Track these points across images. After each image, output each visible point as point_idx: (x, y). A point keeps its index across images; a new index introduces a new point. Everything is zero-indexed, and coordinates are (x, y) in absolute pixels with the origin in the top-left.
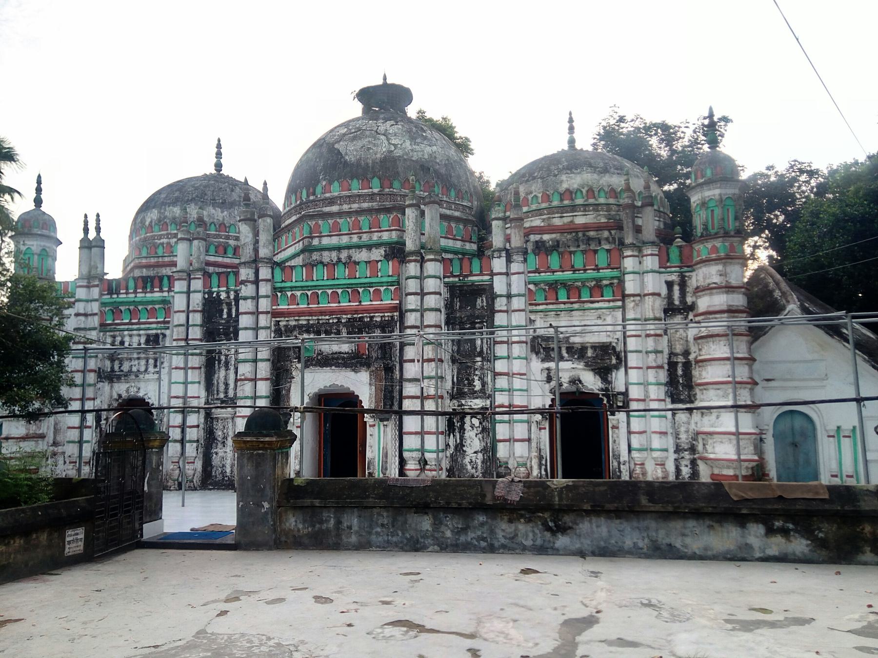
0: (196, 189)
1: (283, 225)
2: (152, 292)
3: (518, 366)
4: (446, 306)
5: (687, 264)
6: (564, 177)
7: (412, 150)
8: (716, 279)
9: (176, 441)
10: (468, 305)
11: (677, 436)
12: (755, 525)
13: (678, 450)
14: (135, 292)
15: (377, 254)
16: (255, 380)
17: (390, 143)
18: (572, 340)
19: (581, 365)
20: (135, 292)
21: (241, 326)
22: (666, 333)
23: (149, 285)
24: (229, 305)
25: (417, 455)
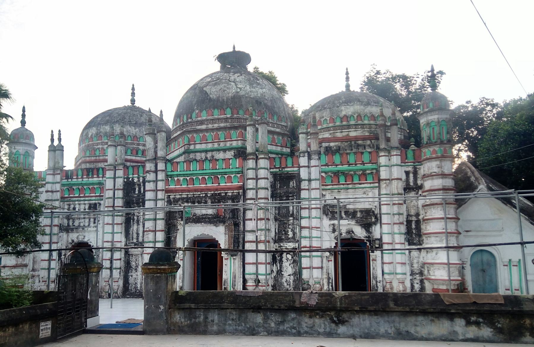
0: (119, 115)
1: (172, 137)
2: (92, 177)
3: (315, 223)
4: (271, 186)
5: (418, 161)
6: (343, 108)
7: (251, 91)
8: (436, 170)
9: (107, 268)
10: (285, 186)
11: (412, 265)
12: (459, 319)
13: (412, 274)
14: (82, 178)
15: (229, 155)
16: (155, 231)
17: (237, 87)
18: (348, 207)
19: (353, 222)
20: (82, 178)
21: (146, 198)
22: (405, 203)
23: (90, 173)
24: (139, 185)
25: (254, 277)
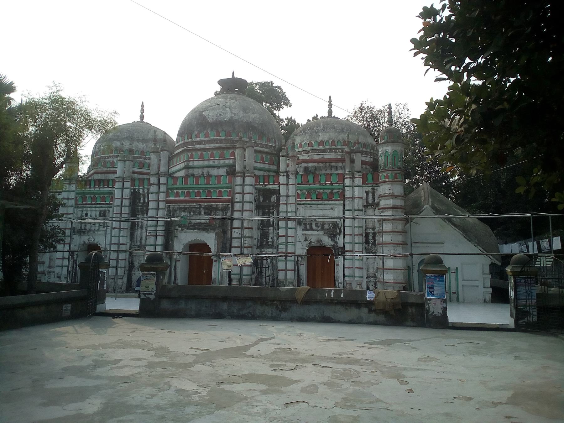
0: (129, 131)
1: (175, 153)
2: (104, 187)
5: (376, 182)
6: (320, 134)
7: (243, 116)
8: (387, 191)
9: (113, 267)
10: (267, 201)
11: (368, 270)
13: (368, 277)
14: (94, 187)
15: (223, 172)
17: (232, 113)
18: (317, 220)
19: (322, 233)
20: (94, 187)
21: (149, 207)
23: (102, 184)
24: (144, 196)
25: (238, 277)
